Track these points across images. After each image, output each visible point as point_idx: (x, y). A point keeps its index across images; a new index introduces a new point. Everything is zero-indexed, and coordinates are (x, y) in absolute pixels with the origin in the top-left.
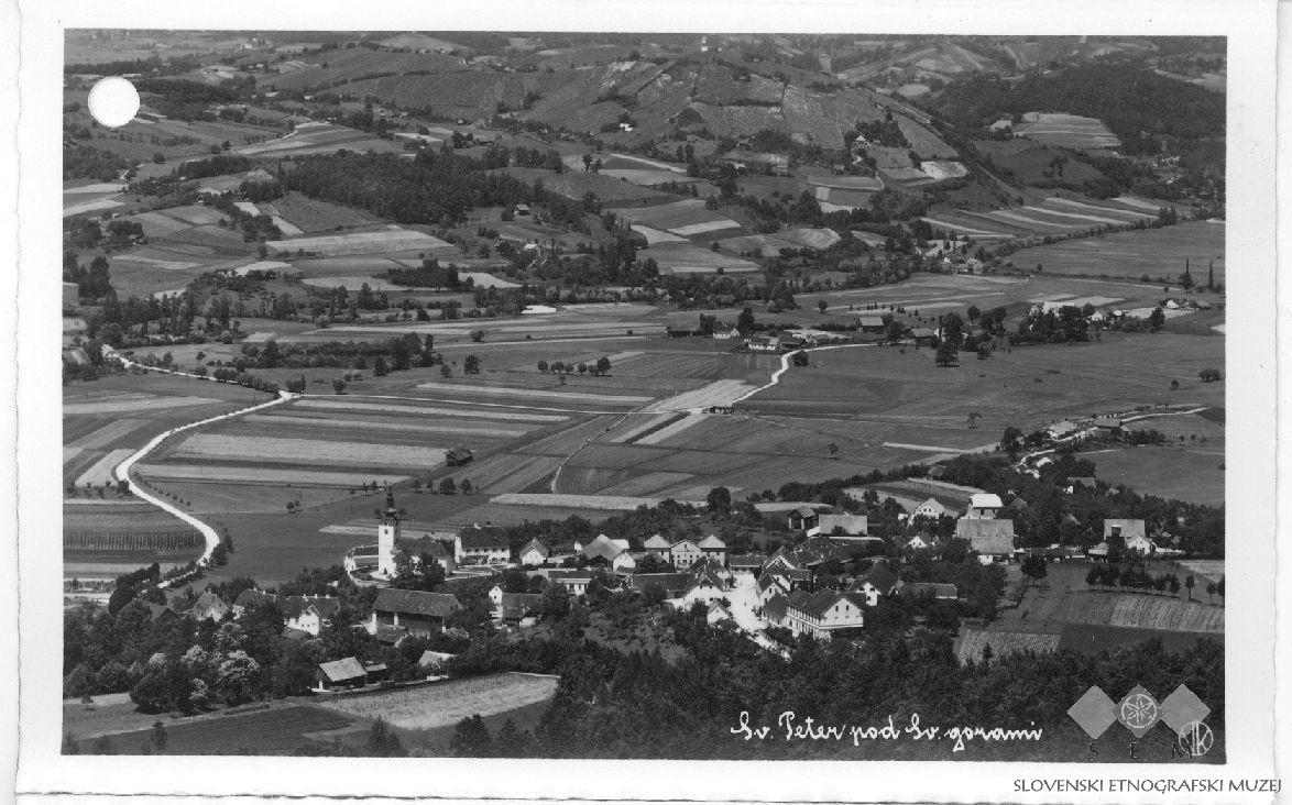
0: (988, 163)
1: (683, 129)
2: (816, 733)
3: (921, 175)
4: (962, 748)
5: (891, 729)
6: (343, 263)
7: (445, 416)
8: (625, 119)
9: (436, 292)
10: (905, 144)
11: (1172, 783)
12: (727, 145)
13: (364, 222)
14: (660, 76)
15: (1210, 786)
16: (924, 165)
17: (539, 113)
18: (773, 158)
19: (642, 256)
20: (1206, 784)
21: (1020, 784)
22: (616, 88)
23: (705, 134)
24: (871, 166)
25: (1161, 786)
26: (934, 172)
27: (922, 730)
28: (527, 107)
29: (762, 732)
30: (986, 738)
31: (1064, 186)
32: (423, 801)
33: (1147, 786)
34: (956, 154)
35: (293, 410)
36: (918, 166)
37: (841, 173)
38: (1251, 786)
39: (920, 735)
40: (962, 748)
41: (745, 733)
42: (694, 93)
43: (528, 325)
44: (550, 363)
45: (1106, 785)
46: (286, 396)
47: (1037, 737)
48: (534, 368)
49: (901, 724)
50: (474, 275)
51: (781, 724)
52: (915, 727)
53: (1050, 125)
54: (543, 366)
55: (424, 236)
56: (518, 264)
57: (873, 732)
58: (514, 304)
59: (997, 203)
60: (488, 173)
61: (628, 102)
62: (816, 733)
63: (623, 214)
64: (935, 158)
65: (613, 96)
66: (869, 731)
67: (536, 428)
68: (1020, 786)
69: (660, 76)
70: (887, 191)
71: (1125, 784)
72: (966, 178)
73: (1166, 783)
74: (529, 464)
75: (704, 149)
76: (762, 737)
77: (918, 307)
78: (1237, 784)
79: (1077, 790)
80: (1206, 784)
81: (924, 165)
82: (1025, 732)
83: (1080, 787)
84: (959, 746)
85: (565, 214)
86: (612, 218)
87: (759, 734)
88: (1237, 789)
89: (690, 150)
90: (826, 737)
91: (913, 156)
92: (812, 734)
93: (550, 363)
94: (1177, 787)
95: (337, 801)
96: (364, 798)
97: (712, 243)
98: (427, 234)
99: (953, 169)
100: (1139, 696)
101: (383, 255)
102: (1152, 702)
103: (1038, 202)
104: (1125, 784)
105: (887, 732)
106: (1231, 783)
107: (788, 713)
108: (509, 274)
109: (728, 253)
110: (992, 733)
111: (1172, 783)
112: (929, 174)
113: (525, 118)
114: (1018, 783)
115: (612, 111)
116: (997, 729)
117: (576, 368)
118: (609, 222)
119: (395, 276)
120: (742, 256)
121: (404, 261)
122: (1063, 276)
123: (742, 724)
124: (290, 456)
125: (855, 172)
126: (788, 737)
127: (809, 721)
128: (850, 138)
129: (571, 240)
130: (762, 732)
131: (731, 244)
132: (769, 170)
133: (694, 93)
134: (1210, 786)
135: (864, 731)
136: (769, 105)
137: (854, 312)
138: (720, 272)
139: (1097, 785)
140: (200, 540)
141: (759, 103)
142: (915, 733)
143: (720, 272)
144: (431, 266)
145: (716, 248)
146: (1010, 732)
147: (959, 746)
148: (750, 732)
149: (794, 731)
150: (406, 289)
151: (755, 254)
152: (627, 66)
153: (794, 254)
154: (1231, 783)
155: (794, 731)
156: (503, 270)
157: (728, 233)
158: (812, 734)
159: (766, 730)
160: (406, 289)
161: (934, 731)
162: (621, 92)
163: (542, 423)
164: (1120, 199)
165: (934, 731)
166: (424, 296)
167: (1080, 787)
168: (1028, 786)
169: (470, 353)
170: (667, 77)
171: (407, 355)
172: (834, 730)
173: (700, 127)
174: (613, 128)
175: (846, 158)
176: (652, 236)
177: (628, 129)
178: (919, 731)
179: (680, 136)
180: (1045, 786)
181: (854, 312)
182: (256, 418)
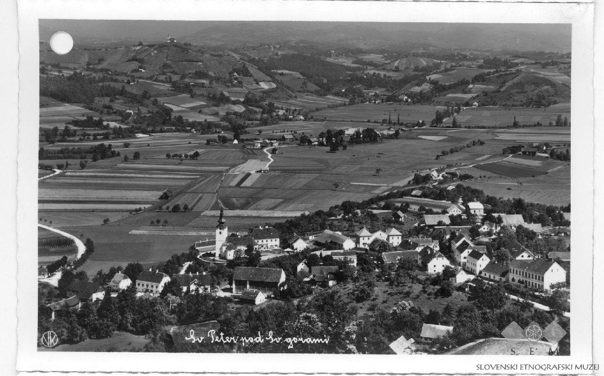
0: (282, 83)
1: (165, 71)
2: (225, 340)
3: (259, 87)
4: (292, 347)
5: (260, 338)
6: (51, 118)
7: (137, 177)
8: (140, 67)
9: (94, 129)
10: (251, 76)
11: (549, 366)
12: (183, 77)
13: (53, 102)
14: (153, 51)
15: (567, 367)
16: (260, 83)
17: (104, 65)
18: (204, 81)
19: (173, 115)
20: (565, 366)
21: (480, 366)
22: (135, 56)
23: (174, 73)
24: (240, 84)
25: (544, 367)
26: (264, 86)
27: (274, 338)
28: (99, 63)
29: (200, 339)
30: (303, 342)
31: (308, 91)
32: (470, 372)
33: (538, 367)
34: (271, 79)
35: (65, 177)
36: (258, 84)
37: (229, 87)
38: (585, 367)
39: (273, 340)
40: (292, 347)
41: (192, 340)
42: (167, 58)
43: (142, 141)
44: (172, 154)
45: (519, 367)
46: (58, 172)
47: (327, 342)
48: (164, 156)
49: (264, 335)
50: (110, 123)
51: (209, 336)
52: (271, 337)
53: (372, 57)
54: (168, 156)
55: (79, 108)
56: (125, 117)
57: (251, 340)
58: (131, 133)
59: (289, 98)
60: (101, 84)
61: (141, 61)
62: (225, 340)
63: (161, 100)
64: (264, 81)
65: (134, 59)
66: (249, 339)
67: (189, 181)
68: (479, 367)
69: (153, 51)
70: (249, 92)
71: (528, 366)
72: (277, 88)
73: (546, 366)
74: (200, 198)
75: (175, 78)
76: (200, 341)
77: (303, 131)
78: (579, 366)
79: (505, 369)
80: (565, 366)
81: (260, 83)
82: (321, 340)
83: (507, 368)
84: (291, 346)
85: (134, 100)
86: (156, 100)
87: (277, 340)
88: (579, 369)
89: (170, 78)
90: (229, 342)
91: (255, 80)
92: (223, 340)
93: (172, 154)
94: (551, 368)
95: (80, 374)
96: (109, 373)
97: (199, 110)
98: (81, 107)
99: (271, 85)
100: (534, 326)
101: (68, 115)
102: (540, 329)
103: (302, 97)
104: (528, 366)
105: (258, 339)
106: (576, 366)
107: (212, 331)
108: (122, 122)
109: (206, 114)
110: (306, 340)
111: (549, 366)
112: (262, 86)
113: (100, 67)
114: (478, 366)
115: (134, 65)
116: (308, 338)
117: (183, 155)
118: (155, 103)
119: (76, 123)
120: (212, 115)
121: (77, 118)
122: (337, 121)
123: (191, 335)
124: (556, 136)
125: (234, 86)
126: (212, 342)
127: (222, 334)
128: (231, 74)
129: (144, 110)
130: (200, 339)
131: (206, 110)
132: (203, 85)
133: (167, 58)
134: (567, 367)
135: (247, 339)
136: (197, 62)
137: (274, 134)
138: (206, 120)
139: (515, 367)
140: (75, 250)
141: (193, 61)
142: (270, 340)
143: (206, 120)
144: (90, 118)
145: (200, 112)
146: (314, 340)
147: (291, 346)
148: (194, 338)
149: (215, 339)
150: (81, 128)
151: (216, 114)
152: (138, 48)
153: (231, 114)
154: (576, 366)
155: (215, 339)
156: (119, 120)
157: (203, 106)
158: (223, 340)
159: (202, 338)
160: (81, 128)
161: (280, 339)
162: (138, 57)
163: (192, 179)
164: (327, 97)
165: (280, 339)
166: (91, 131)
167: (507, 368)
168: (483, 367)
169: (136, 151)
170: (156, 52)
171: (103, 153)
172: (233, 338)
173: (172, 70)
174: (136, 71)
175: (231, 82)
176: (175, 108)
177: (143, 71)
178: (272, 339)
179: (164, 73)
180: (491, 367)
181: (274, 134)
182: (52, 181)
